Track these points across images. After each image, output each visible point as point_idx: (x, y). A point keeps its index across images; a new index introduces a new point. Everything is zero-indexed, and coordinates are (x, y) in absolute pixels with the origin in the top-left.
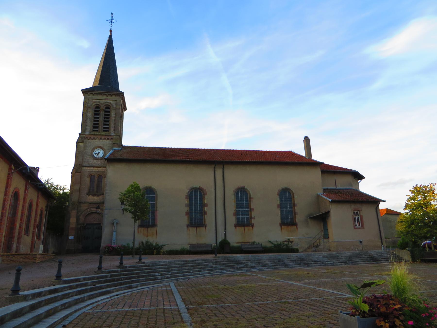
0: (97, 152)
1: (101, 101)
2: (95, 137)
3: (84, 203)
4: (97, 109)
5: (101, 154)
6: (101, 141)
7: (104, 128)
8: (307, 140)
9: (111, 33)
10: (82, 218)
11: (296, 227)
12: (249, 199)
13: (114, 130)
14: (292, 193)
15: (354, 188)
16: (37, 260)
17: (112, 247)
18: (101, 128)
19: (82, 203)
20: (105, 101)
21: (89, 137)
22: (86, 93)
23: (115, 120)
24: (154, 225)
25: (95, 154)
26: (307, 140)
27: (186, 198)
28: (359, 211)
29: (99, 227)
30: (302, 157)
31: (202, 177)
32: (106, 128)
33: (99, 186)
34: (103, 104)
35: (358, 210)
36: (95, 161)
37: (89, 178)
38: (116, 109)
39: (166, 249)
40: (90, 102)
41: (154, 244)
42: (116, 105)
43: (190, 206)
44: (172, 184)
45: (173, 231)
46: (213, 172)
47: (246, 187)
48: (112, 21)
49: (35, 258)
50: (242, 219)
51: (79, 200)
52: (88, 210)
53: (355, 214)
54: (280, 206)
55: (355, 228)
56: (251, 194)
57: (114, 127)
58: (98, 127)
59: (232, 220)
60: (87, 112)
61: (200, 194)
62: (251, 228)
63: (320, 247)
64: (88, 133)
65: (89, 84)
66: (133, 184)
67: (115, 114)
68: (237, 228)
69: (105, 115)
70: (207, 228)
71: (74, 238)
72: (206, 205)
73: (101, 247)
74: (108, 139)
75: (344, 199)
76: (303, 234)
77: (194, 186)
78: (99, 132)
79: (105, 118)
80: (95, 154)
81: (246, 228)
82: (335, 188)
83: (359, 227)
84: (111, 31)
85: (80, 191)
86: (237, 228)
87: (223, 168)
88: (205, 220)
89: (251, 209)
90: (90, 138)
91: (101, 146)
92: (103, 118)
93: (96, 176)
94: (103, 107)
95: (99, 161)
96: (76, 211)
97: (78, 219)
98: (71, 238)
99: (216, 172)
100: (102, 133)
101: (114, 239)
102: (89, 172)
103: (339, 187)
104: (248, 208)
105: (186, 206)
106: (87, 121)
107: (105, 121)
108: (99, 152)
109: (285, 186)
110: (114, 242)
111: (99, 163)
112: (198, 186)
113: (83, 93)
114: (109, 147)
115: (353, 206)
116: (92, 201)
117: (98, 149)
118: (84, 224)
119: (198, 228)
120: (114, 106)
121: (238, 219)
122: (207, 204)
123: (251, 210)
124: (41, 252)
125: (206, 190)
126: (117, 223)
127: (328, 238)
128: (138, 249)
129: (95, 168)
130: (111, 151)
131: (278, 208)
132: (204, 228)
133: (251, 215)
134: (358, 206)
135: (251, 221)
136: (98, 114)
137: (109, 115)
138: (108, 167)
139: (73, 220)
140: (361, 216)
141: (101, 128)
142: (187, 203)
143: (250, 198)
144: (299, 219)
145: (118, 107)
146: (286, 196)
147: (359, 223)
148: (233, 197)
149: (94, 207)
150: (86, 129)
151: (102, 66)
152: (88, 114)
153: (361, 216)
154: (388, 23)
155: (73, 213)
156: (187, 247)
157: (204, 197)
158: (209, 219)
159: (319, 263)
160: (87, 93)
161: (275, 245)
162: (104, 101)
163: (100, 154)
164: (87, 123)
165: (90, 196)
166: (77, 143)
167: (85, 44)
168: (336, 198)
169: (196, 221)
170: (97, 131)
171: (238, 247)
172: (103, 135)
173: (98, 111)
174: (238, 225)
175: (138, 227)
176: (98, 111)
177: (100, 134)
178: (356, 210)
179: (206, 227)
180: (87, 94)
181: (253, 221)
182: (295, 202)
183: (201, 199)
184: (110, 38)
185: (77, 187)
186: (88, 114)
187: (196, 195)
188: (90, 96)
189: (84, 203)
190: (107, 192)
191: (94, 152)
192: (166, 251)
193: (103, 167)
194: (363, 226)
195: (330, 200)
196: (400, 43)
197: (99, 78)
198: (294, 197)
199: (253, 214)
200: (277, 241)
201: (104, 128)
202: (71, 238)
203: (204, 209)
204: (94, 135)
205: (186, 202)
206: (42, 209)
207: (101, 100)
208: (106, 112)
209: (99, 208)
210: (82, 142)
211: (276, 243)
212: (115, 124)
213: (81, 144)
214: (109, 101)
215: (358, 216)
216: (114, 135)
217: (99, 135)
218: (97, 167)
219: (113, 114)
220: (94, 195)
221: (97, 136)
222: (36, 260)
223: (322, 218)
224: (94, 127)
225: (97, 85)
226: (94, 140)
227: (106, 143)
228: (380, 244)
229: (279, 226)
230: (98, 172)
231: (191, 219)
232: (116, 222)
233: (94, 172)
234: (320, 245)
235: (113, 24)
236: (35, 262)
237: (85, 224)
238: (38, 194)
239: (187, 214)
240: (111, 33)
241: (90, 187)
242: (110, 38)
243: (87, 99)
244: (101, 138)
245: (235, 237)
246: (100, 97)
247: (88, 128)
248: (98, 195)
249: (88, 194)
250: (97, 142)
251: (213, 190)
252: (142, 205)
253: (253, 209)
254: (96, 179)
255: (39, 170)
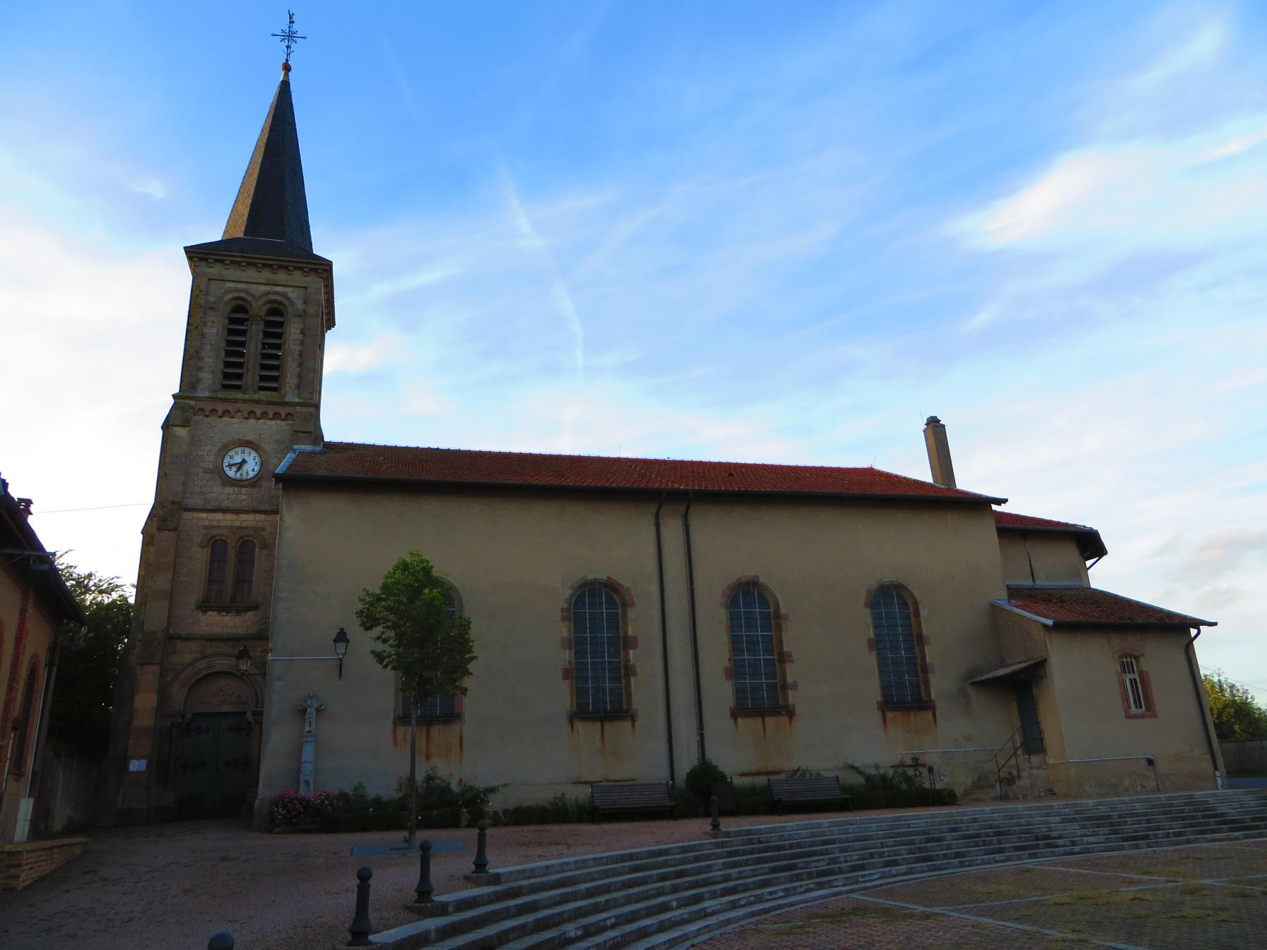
0: (238, 459)
1: (253, 288)
2: (230, 407)
3: (188, 638)
4: (238, 314)
5: (252, 466)
6: (252, 421)
7: (263, 378)
8: (935, 430)
9: (286, 75)
10: (178, 693)
11: (930, 714)
12: (774, 620)
13: (298, 387)
14: (910, 602)
15: (1077, 583)
16: (23, 876)
17: (301, 801)
18: (251, 376)
19: (180, 638)
20: (269, 288)
21: (208, 407)
22: (201, 259)
23: (301, 352)
24: (452, 716)
25: (230, 466)
26: (935, 430)
27: (564, 619)
28: (1136, 658)
29: (247, 726)
30: (923, 484)
31: (617, 546)
32: (271, 376)
33: (243, 580)
34: (258, 307)
35: (1131, 656)
36: (229, 490)
37: (207, 551)
38: (303, 315)
39: (495, 804)
40: (216, 289)
41: (455, 787)
42: (305, 302)
43: (577, 644)
44: (509, 574)
45: (516, 740)
46: (652, 529)
47: (762, 580)
48: (290, 36)
49: (12, 871)
50: (756, 689)
51: (167, 628)
52: (201, 665)
53: (1126, 668)
54: (876, 644)
55: (1128, 716)
56: (782, 605)
57: (299, 376)
58: (239, 377)
59: (720, 693)
60: (205, 324)
61: (611, 603)
62: (785, 719)
63: (1021, 783)
64: (207, 394)
65: (214, 234)
66: (408, 560)
67: (302, 332)
68: (740, 720)
69: (267, 335)
70: (637, 724)
71: (148, 766)
72: (630, 643)
73: (257, 802)
74: (277, 416)
75: (1081, 619)
76: (958, 738)
77: (591, 577)
78: (245, 392)
79: (264, 345)
80: (230, 466)
81: (770, 721)
82: (1029, 583)
83: (1140, 711)
84: (287, 68)
85: (172, 595)
86: (740, 720)
87: (686, 517)
88: (629, 695)
89: (781, 654)
90: (214, 410)
91: (251, 437)
92: (260, 346)
93: (232, 542)
94: (259, 309)
95: (244, 490)
96: (157, 668)
97: (163, 695)
98: (136, 765)
99: (663, 530)
100: (256, 397)
101: (307, 768)
102: (205, 527)
103: (1040, 583)
104: (771, 652)
105: (563, 647)
106: (203, 354)
107: (264, 356)
108: (244, 462)
109: (889, 577)
110: (307, 782)
111: (244, 497)
112: (602, 576)
113: (190, 258)
114: (277, 441)
115: (1117, 643)
116: (217, 630)
117: (239, 449)
118: (183, 717)
119: (607, 726)
120: (300, 306)
121: (740, 692)
122: (635, 638)
123: (783, 658)
124: (22, 830)
125: (629, 590)
126: (318, 710)
127: (1042, 750)
128: (402, 805)
129: (229, 516)
130: (290, 457)
131: (870, 650)
132: (629, 724)
133: (784, 675)
134: (1131, 642)
135: (786, 698)
136: (243, 333)
137: (279, 336)
138: (284, 509)
139: (145, 701)
140: (1141, 674)
141: (251, 376)
142: (565, 635)
143: (778, 615)
144: (941, 685)
145: (311, 310)
146: (892, 604)
147: (1141, 698)
148: (722, 614)
149: (230, 655)
150: (199, 380)
151: (255, 176)
152: (206, 330)
153: (1141, 674)
154: (1008, 158)
155: (148, 677)
156: (582, 794)
157: (625, 615)
158: (645, 692)
159: (1061, 842)
160: (206, 260)
161: (868, 779)
162: (263, 288)
163: (246, 467)
164: (201, 359)
165: (210, 613)
166: (166, 427)
167: (156, 189)
168: (1066, 617)
169: (600, 697)
170: (238, 387)
171: (752, 790)
172: (257, 402)
173: (241, 322)
174: (740, 711)
175: (394, 723)
176: (241, 322)
177: (247, 397)
178: (1126, 656)
179: (633, 720)
180: (203, 264)
181: (792, 697)
182: (925, 632)
183: (615, 622)
184: (285, 89)
185: (163, 581)
186: (206, 330)
187: (597, 610)
188: (217, 270)
189: (188, 638)
190: (282, 595)
191: (227, 461)
192: (505, 811)
193: (259, 512)
194: (1150, 709)
195: (1050, 622)
196: (1033, 211)
197: (245, 211)
198: (917, 614)
199: (792, 673)
200: (877, 767)
201: (263, 378)
202: (136, 765)
203: (627, 655)
204: (226, 400)
205: (564, 630)
206: (35, 657)
207: (255, 284)
208: (268, 324)
209: (249, 657)
210: (185, 424)
211: (873, 772)
212: (300, 365)
213: (181, 432)
214: (280, 289)
215: (1132, 676)
216: (299, 404)
217: (244, 401)
218: (237, 512)
219: (293, 331)
220: (222, 609)
221: (239, 405)
222: (16, 877)
223: (1021, 687)
224: (226, 376)
225: (240, 233)
226: (225, 419)
227: (268, 430)
228: (1210, 767)
229: (878, 715)
230: (239, 528)
231: (580, 693)
232: (316, 705)
233: (226, 527)
234: (1019, 776)
235: (293, 45)
236: (12, 889)
237: (189, 716)
238: (25, 599)
239: (567, 674)
240: (286, 75)
241: (210, 581)
242: (285, 89)
243: (205, 280)
244: (252, 412)
245: (737, 754)
246: (251, 274)
247: (206, 377)
248: (239, 612)
249: (204, 607)
250: (238, 427)
251: (654, 589)
252: (425, 640)
253: (790, 655)
254: (232, 555)
255: (32, 508)
